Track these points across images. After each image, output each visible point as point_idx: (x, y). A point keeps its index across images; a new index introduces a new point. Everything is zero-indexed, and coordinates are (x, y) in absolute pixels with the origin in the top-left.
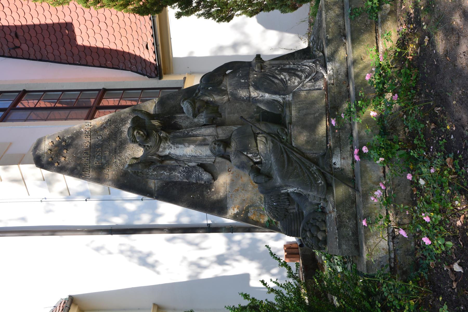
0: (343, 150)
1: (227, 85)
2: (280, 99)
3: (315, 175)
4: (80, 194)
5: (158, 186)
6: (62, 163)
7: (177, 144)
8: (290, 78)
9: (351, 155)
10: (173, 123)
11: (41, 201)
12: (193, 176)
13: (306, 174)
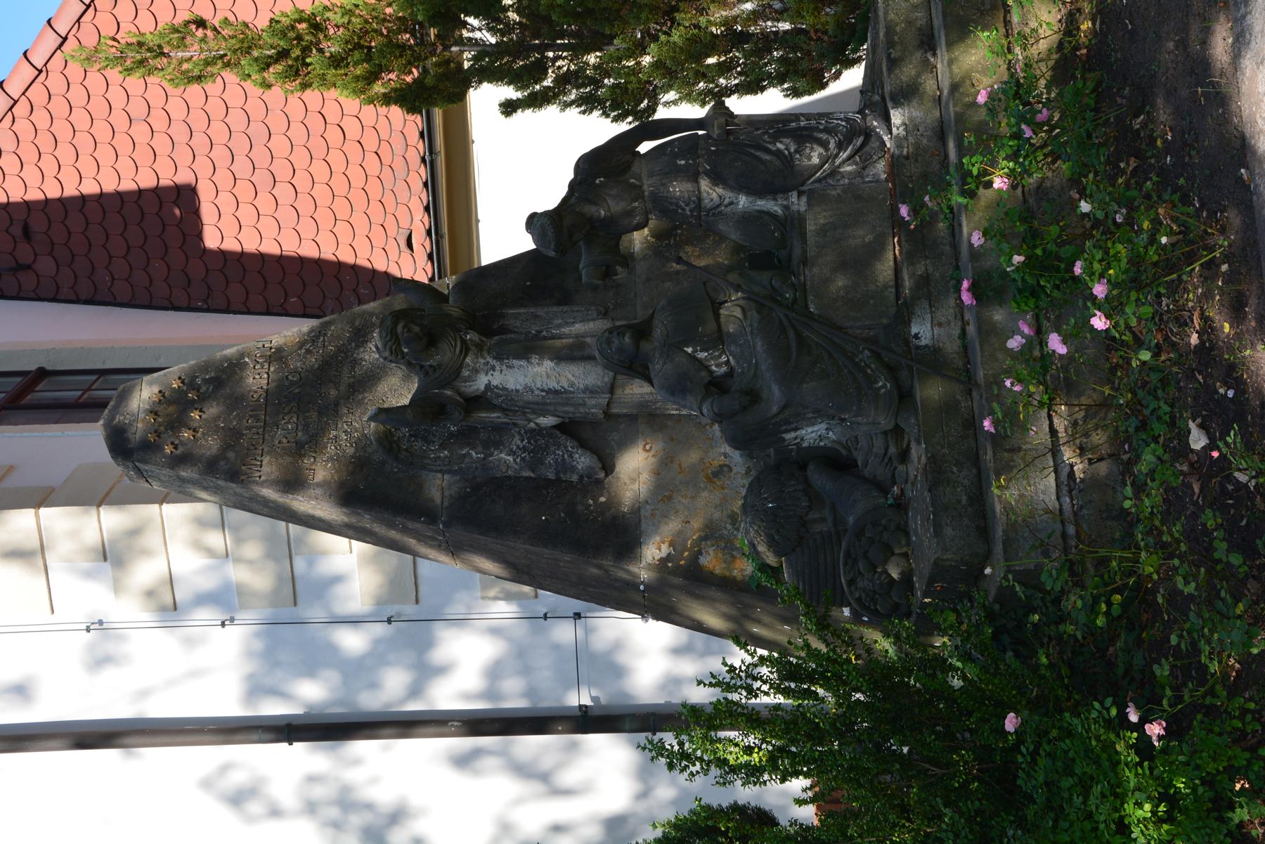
0: (936, 304)
1: (643, 175)
2: (776, 208)
3: (869, 371)
4: (205, 599)
5: (451, 495)
6: (186, 444)
7: (508, 359)
8: (799, 148)
9: (959, 315)
10: (495, 327)
11: (88, 630)
12: (549, 459)
13: (845, 371)
